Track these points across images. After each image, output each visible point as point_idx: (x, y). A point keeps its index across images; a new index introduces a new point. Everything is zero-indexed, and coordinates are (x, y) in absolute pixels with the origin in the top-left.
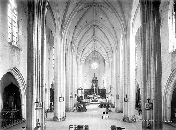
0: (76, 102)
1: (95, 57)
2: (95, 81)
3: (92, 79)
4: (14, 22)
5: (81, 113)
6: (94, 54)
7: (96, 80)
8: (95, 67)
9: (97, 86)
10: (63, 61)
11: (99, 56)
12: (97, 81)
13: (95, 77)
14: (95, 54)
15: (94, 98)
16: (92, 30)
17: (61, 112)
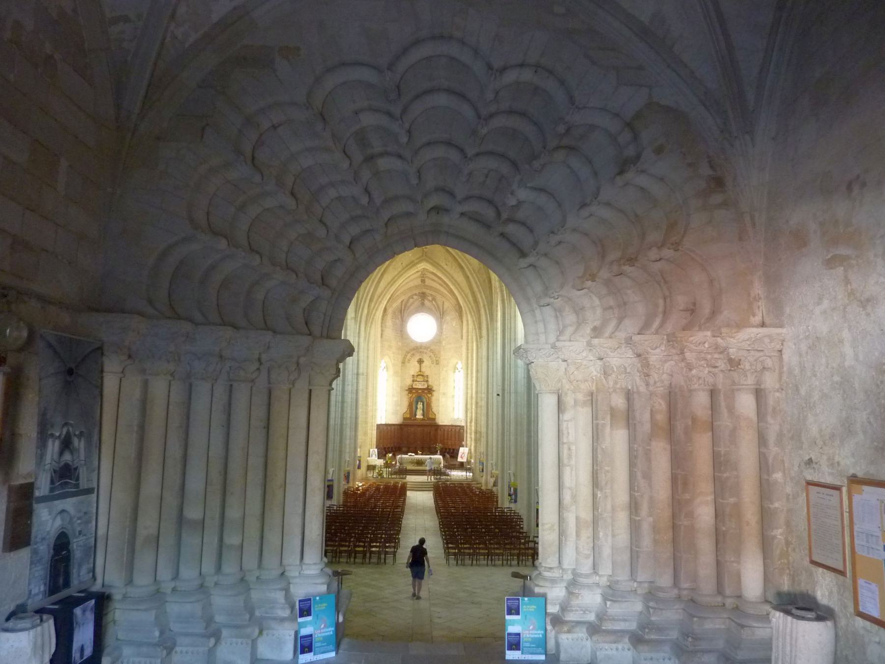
1: (423, 293)
2: (420, 394)
3: (409, 382)
6: (418, 282)
9: (428, 408)
12: (429, 390)
13: (421, 374)
14: (423, 281)
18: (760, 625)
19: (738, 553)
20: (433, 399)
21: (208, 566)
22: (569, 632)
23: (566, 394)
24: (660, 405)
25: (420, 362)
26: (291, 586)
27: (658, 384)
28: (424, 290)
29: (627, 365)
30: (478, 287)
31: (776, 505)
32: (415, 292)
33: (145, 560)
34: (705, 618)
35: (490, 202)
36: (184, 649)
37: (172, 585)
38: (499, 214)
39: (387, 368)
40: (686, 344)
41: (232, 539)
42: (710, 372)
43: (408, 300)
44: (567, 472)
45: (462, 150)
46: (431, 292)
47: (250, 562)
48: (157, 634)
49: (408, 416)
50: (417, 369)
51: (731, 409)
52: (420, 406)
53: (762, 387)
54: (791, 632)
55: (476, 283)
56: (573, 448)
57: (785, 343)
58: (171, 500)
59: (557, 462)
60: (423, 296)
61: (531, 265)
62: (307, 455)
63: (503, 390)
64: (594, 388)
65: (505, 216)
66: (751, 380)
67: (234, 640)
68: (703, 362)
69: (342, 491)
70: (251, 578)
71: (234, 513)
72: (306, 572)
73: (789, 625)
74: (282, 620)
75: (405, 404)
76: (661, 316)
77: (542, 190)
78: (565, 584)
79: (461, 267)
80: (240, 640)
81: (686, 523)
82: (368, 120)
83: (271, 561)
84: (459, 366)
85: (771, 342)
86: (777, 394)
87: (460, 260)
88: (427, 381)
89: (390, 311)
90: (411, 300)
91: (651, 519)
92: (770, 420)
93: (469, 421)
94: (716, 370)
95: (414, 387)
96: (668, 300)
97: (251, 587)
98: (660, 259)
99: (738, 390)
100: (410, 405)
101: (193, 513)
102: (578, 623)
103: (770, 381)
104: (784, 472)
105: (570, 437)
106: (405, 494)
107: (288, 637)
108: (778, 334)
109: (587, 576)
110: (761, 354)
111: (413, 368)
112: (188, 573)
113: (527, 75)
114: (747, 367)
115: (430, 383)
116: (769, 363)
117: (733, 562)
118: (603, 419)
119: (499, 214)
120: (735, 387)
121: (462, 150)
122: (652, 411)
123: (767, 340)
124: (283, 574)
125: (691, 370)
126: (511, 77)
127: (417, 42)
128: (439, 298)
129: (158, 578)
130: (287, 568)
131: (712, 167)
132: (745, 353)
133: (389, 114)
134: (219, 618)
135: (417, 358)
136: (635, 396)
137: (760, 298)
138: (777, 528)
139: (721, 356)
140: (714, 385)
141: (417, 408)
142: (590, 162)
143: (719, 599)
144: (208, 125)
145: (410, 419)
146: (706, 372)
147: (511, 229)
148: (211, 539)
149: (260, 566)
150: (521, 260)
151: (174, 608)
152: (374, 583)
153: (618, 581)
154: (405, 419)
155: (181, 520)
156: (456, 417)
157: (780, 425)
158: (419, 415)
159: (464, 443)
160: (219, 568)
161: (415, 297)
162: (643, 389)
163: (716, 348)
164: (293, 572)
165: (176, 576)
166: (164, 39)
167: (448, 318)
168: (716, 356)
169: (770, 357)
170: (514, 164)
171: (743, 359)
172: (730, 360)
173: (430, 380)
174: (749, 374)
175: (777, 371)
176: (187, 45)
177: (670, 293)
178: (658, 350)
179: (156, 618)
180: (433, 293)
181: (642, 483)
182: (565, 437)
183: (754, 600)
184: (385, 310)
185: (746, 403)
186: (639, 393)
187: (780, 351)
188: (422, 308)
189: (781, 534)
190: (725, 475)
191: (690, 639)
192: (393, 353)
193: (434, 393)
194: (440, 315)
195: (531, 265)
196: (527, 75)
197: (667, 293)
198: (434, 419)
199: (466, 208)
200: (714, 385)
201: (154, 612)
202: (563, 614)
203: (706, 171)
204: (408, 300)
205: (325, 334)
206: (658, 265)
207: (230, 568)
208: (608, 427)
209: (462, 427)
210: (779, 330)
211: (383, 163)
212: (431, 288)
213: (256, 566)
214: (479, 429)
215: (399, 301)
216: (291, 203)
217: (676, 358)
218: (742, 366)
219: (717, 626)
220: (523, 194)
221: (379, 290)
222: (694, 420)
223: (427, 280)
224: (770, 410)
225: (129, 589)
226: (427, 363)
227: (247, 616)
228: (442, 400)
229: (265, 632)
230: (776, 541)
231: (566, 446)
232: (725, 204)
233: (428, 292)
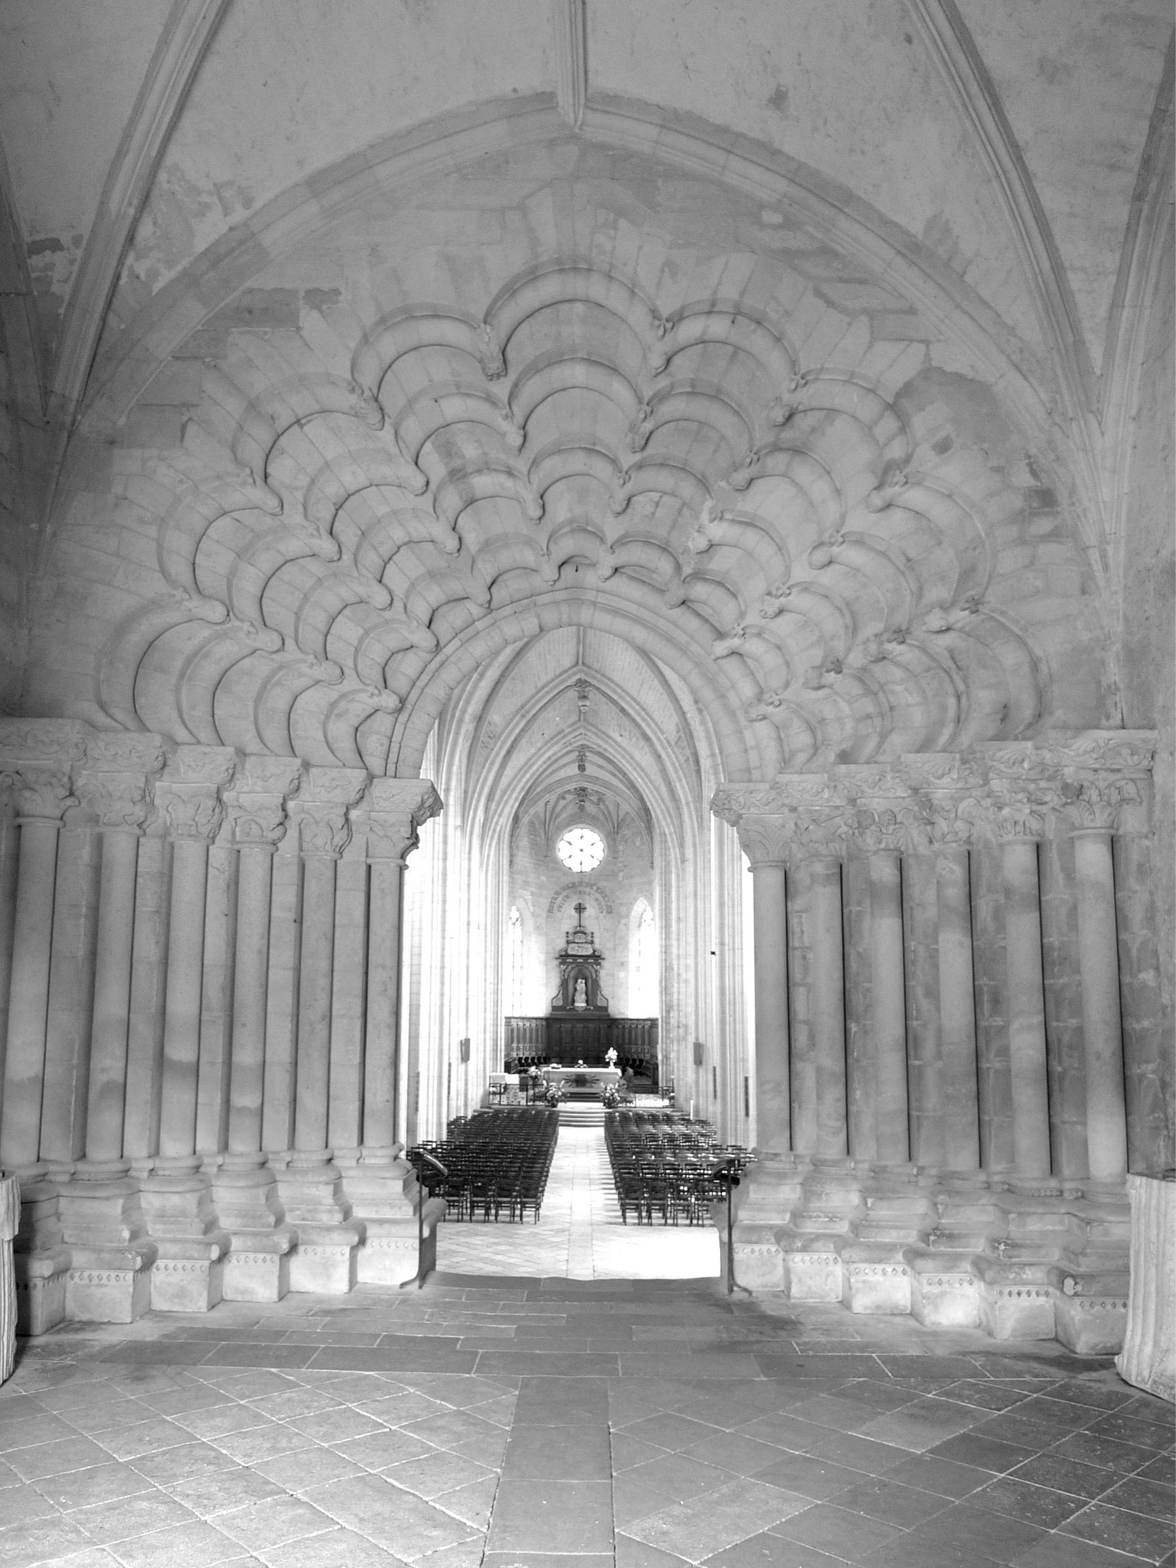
0: (409, 1165)
1: (583, 790)
3: (561, 944)
4: (194, 741)
5: (946, 454)
6: (574, 770)
7: (590, 952)
8: (589, 850)
9: (593, 989)
10: (414, 1078)
11: (615, 781)
12: (596, 958)
13: (580, 931)
14: (582, 768)
15: (1071, 414)
17: (1139, 1321)
18: (1119, 1219)
19: (1082, 1108)
20: (603, 974)
21: (207, 1142)
22: (804, 1249)
23: (798, 867)
24: (953, 871)
25: (580, 909)
26: (344, 1181)
27: (949, 838)
28: (585, 785)
29: (896, 810)
30: (676, 772)
31: (1146, 1024)
32: (567, 787)
33: (104, 1121)
34: (1030, 1214)
35: (664, 549)
36: (171, 1263)
37: (150, 1164)
38: (678, 567)
39: (521, 920)
40: (990, 763)
41: (245, 1099)
42: (1032, 812)
43: (556, 803)
44: (799, 995)
45: (614, 461)
46: (596, 788)
47: (276, 1138)
48: (126, 1234)
49: (561, 1003)
50: (576, 923)
51: (1070, 873)
52: (581, 985)
53: (1121, 831)
54: (1159, 1202)
55: (673, 764)
56: (810, 956)
57: (1157, 757)
58: (144, 1030)
59: (784, 980)
61: (733, 653)
62: (367, 973)
63: (722, 944)
64: (844, 854)
65: (687, 570)
66: (1101, 819)
67: (252, 1255)
68: (1020, 796)
69: (445, 1122)
70: (278, 1166)
71: (246, 1056)
72: (367, 1161)
73: (1155, 1193)
74: (329, 1229)
75: (555, 981)
76: (952, 725)
77: (750, 524)
78: (799, 1179)
79: (647, 739)
80: (261, 1256)
81: (997, 1065)
82: (454, 407)
83: (309, 1137)
84: (648, 915)
85: (1132, 754)
86: (1147, 843)
87: (643, 725)
88: (592, 942)
89: (525, 820)
90: (562, 803)
91: (940, 1064)
92: (1133, 884)
94: (1043, 809)
95: (570, 952)
96: (964, 699)
97: (278, 1178)
98: (948, 629)
99: (1080, 837)
100: (564, 984)
101: (180, 1051)
102: (818, 1237)
103: (1132, 821)
104: (1157, 969)
105: (805, 937)
106: (554, 1134)
107: (338, 1257)
108: (1144, 741)
109: (835, 1163)
110: (1118, 776)
111: (568, 920)
112: (174, 1148)
113: (718, 327)
114: (1095, 797)
115: (597, 946)
116: (1130, 790)
117: (1076, 1123)
118: (859, 904)
119: (678, 567)
120: (1075, 833)
121: (614, 461)
122: (938, 883)
123: (1125, 751)
124: (330, 1160)
125: (1000, 809)
126: (689, 330)
127: (532, 275)
128: (609, 795)
129: (125, 1154)
130: (336, 1153)
131: (1034, 473)
132: (1090, 776)
133: (490, 399)
134: (226, 1223)
135: (574, 904)
136: (911, 861)
137: (1118, 689)
138: (1147, 1062)
139: (1052, 784)
140: (1042, 835)
141: (575, 990)
142: (829, 473)
143: (1053, 1183)
144: (190, 419)
145: (562, 1008)
146: (1027, 811)
147: (700, 590)
148: (211, 1098)
149: (292, 1146)
150: (718, 643)
151: (151, 1200)
152: (499, 1257)
153: (886, 1167)
154: (554, 1008)
155: (161, 1061)
157: (1152, 893)
158: (580, 1004)
160: (225, 1147)
161: (569, 797)
162: (923, 849)
163: (1043, 771)
164: (344, 1161)
165: (156, 1152)
166: (118, 277)
168: (1043, 784)
169: (1133, 780)
170: (703, 483)
171: (1085, 784)
172: (1066, 787)
173: (597, 941)
174: (1097, 810)
175: (1145, 804)
176: (155, 290)
177: (967, 686)
178: (946, 780)
179: (124, 1211)
180: (602, 790)
181: (922, 1003)
182: (796, 937)
183: (1109, 1180)
184: (516, 819)
185: (1092, 858)
186: (917, 856)
187: (1150, 771)
188: (580, 818)
189: (1153, 1072)
190: (1061, 981)
191: (1002, 1247)
192: (532, 894)
193: (603, 963)
194: (613, 832)
195: (733, 653)
196: (718, 327)
197: (961, 687)
198: (606, 1009)
199: (622, 556)
200: (1042, 835)
201: (120, 1202)
202: (796, 1226)
203: (1024, 479)
204: (556, 803)
205: (391, 772)
206: (947, 640)
207: (242, 1145)
208: (868, 916)
209: (653, 1022)
210: (1147, 734)
211: (482, 483)
213: (285, 1147)
214: (683, 1020)
215: (541, 803)
216: (326, 546)
217: (977, 792)
218: (1086, 797)
219: (1050, 1227)
220: (717, 531)
221: (504, 781)
222: (1008, 892)
223: (587, 765)
224: (1134, 867)
225: (81, 1167)
226: (591, 911)
227: (272, 1220)
229: (301, 1249)
230: (1145, 1083)
231: (798, 953)
232: (1055, 535)
233: (590, 787)
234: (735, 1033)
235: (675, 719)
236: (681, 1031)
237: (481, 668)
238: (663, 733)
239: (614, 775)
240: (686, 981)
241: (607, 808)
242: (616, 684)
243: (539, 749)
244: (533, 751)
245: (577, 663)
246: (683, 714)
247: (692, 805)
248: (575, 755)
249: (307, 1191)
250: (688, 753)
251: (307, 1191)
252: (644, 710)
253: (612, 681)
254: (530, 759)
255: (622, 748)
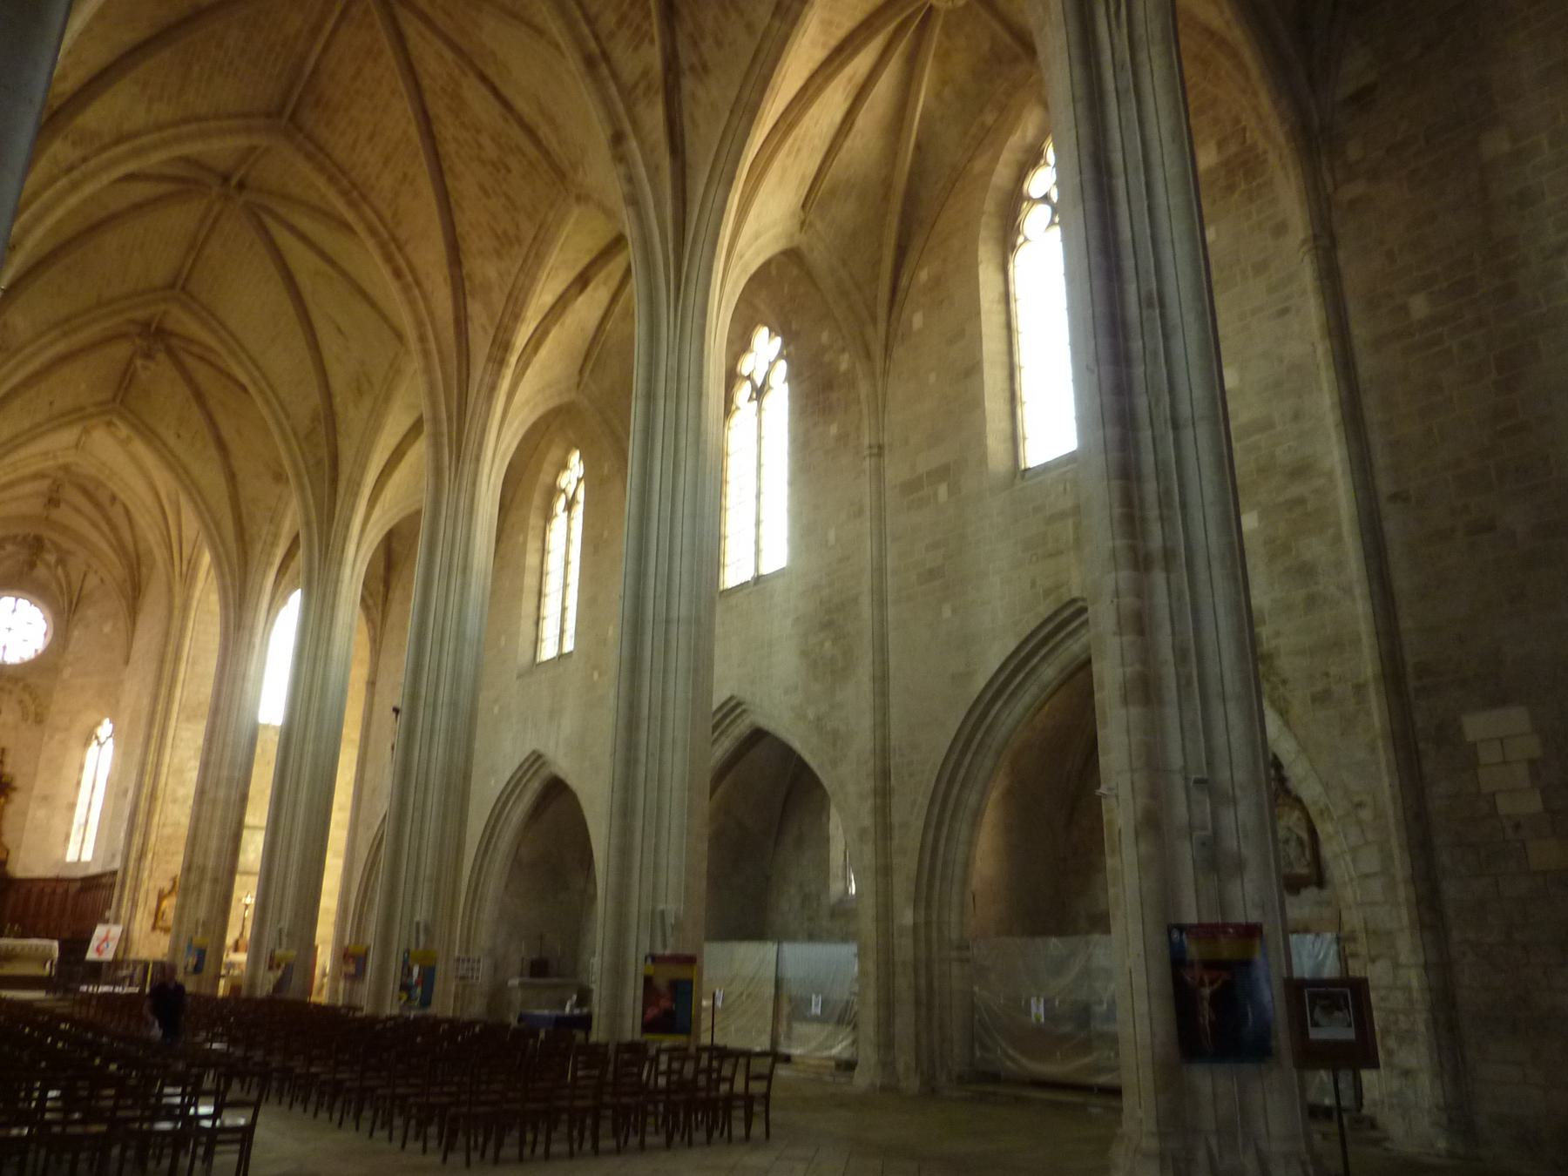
6: (35, 507)
11: (94, 536)
14: (53, 501)
16: (181, 219)
60: (36, 545)
63: (413, 696)
93: (134, 855)
156: (71, 857)
159: (109, 914)
161: (10, 548)
167: (91, 613)
180: (66, 543)
193: (17, 798)
194: (67, 612)
212: (65, 529)
228: (38, 814)
233: (47, 534)
234: (421, 838)
235: (316, 399)
236: (194, 877)
237: (76, 174)
238: (288, 417)
239: (95, 525)
240: (214, 802)
241: (67, 576)
242: (231, 334)
243: (39, 425)
244: (26, 424)
245: (172, 286)
246: (328, 394)
247: (315, 526)
248: (44, 485)
249: (1001, 732)
250: (324, 452)
251: (1001, 732)
252: (264, 377)
253: (224, 327)
254: (17, 436)
255: (174, 455)
